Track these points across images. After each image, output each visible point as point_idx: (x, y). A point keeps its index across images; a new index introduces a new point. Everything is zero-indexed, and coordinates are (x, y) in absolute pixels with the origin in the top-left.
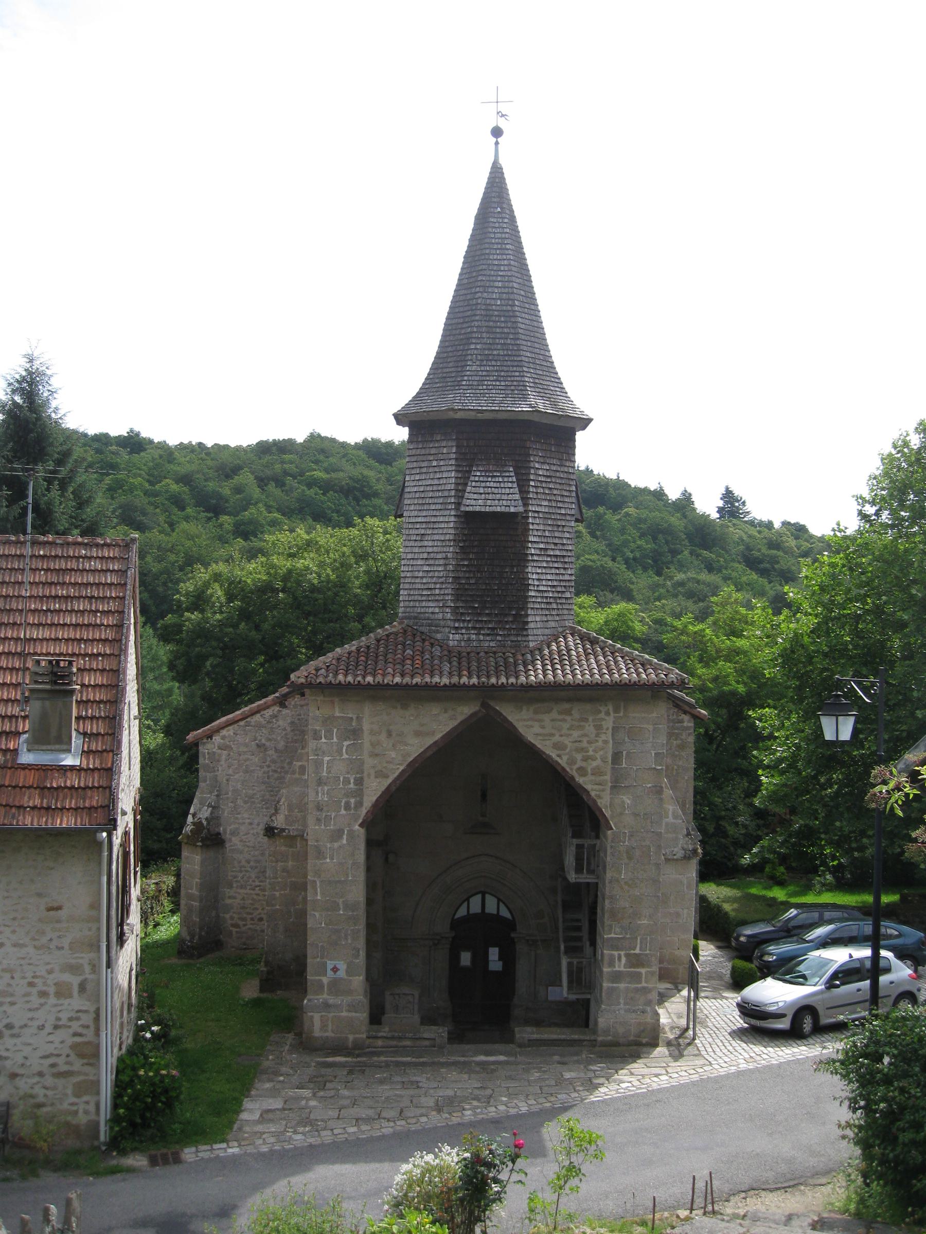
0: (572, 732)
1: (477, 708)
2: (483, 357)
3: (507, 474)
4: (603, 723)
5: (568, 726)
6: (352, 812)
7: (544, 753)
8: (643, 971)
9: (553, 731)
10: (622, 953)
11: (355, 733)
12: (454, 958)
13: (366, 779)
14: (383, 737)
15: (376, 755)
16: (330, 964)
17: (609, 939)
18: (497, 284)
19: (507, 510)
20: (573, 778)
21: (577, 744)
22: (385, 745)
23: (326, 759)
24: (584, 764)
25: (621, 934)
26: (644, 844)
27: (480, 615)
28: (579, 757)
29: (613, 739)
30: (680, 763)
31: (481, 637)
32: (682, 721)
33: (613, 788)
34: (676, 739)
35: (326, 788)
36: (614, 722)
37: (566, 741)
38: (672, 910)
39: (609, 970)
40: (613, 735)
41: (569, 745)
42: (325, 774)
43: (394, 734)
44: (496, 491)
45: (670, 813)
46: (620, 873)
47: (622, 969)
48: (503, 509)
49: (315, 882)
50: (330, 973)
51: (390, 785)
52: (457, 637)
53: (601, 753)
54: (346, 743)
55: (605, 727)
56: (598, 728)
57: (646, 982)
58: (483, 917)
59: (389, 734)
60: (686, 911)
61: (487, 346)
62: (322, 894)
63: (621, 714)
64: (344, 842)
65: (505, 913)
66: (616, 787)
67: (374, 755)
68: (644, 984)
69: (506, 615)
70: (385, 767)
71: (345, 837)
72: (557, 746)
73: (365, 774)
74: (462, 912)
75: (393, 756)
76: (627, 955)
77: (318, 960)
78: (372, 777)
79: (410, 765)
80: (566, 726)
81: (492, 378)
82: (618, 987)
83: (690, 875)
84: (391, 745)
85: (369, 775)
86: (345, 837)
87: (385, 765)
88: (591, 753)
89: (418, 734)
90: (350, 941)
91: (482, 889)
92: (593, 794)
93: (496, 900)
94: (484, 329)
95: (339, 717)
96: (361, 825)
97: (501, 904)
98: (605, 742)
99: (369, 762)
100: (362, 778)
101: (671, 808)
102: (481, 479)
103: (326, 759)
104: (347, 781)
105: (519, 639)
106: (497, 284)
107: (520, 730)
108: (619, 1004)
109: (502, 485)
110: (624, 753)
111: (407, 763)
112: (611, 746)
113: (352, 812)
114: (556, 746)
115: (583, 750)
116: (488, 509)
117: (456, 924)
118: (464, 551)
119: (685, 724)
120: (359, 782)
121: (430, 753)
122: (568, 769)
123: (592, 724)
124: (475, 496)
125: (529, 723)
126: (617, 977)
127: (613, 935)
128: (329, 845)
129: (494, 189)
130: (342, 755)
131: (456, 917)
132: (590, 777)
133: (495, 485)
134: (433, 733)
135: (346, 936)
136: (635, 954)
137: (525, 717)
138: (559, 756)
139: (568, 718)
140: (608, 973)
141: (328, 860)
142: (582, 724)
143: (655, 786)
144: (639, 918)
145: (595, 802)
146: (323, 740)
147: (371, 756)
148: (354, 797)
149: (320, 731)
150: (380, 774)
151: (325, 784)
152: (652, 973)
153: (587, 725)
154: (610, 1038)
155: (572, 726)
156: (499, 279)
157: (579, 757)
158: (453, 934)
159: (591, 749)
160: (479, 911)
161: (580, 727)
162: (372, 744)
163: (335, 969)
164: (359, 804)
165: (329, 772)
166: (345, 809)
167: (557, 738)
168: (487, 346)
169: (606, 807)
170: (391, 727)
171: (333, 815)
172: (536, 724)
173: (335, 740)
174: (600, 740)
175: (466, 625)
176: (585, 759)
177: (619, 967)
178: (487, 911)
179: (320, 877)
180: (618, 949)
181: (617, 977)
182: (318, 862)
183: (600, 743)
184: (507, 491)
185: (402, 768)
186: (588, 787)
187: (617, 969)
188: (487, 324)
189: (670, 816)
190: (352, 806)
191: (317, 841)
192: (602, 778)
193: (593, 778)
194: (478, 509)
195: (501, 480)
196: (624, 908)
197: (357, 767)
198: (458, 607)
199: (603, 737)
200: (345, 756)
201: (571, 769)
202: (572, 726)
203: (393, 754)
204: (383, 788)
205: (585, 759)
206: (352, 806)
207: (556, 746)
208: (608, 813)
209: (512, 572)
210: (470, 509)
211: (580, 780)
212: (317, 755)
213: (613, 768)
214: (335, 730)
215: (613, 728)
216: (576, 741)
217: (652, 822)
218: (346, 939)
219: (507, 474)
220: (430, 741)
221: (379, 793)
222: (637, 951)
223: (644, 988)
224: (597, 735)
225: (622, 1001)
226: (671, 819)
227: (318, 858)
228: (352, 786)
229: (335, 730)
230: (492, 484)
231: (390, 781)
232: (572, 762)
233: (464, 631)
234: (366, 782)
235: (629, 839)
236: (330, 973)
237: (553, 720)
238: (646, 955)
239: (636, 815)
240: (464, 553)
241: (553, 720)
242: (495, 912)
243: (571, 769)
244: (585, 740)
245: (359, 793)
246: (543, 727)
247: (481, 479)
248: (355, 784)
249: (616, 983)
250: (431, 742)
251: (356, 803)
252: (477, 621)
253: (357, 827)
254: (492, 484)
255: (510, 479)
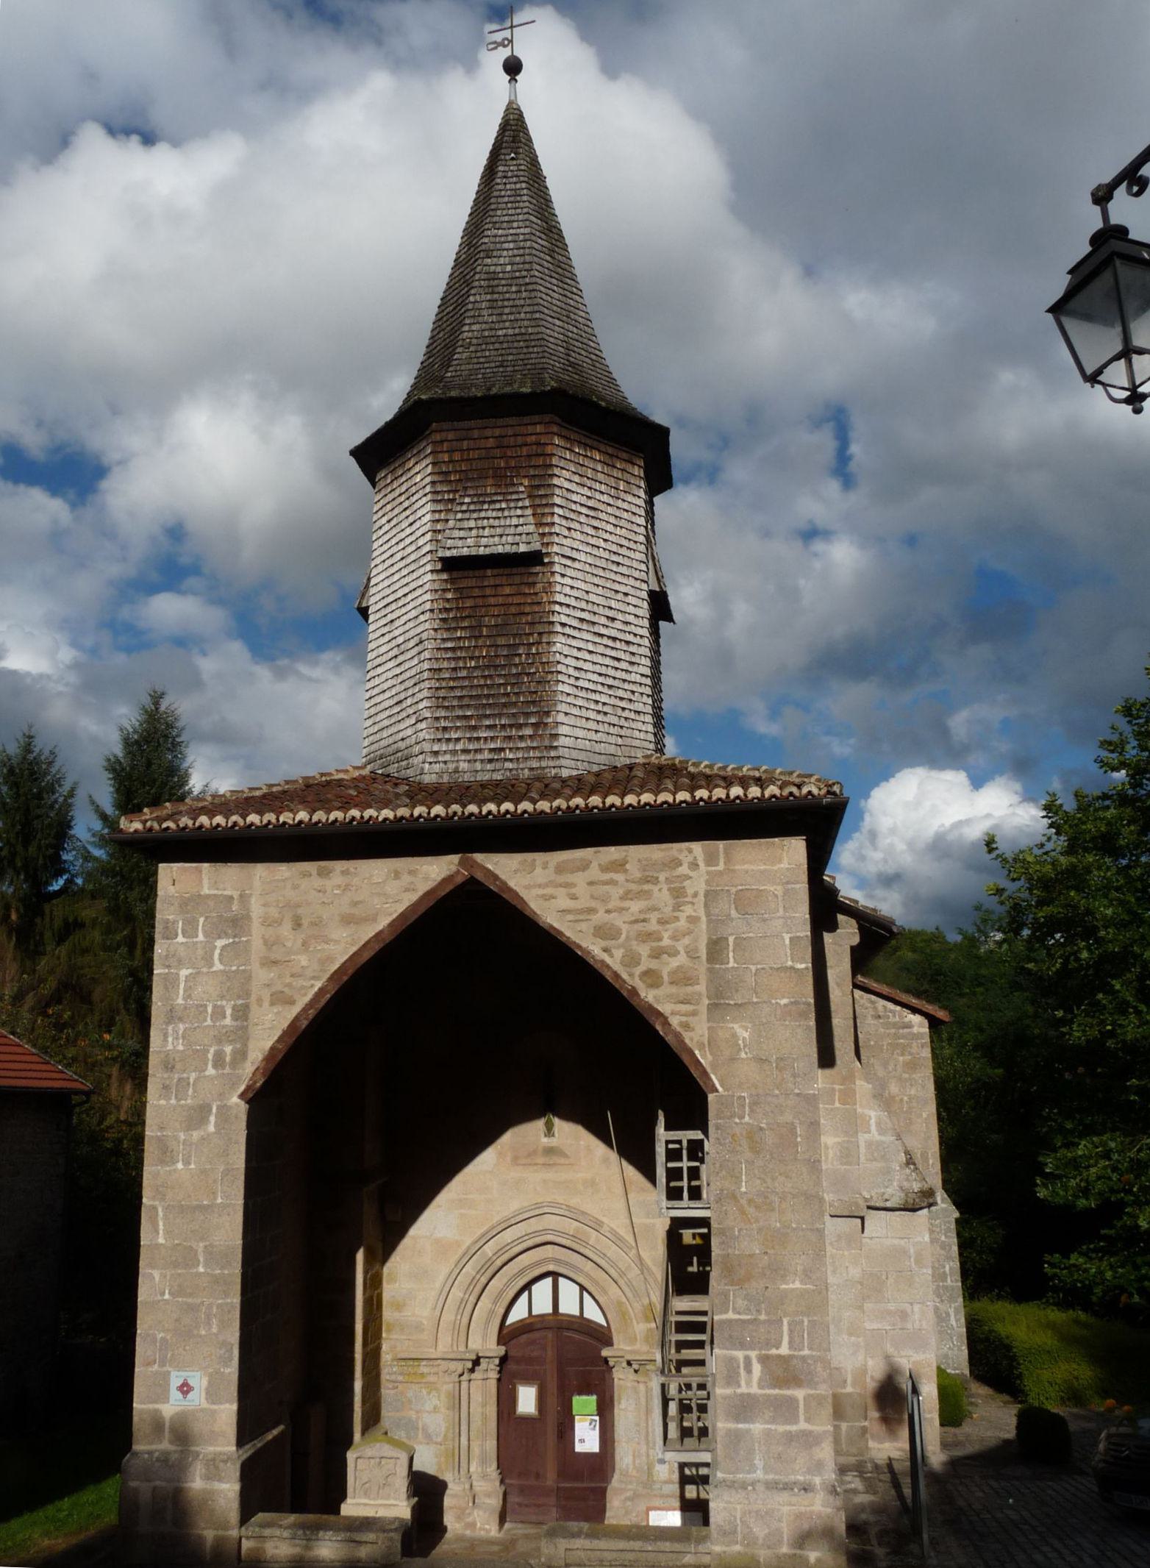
0: (627, 904)
1: (454, 868)
2: (480, 341)
3: (514, 497)
4: (687, 883)
5: (621, 891)
6: (227, 1070)
7: (579, 947)
8: (799, 1394)
9: (593, 904)
10: (753, 1354)
11: (236, 924)
12: (506, 1400)
13: (254, 1007)
14: (286, 930)
15: (275, 962)
16: (175, 1381)
17: (722, 1322)
18: (506, 246)
19: (514, 549)
20: (634, 992)
21: (639, 927)
22: (289, 944)
23: (184, 973)
24: (653, 965)
25: (748, 1311)
26: (781, 1119)
27: (475, 728)
28: (644, 950)
29: (708, 914)
30: (913, 1092)
31: (478, 766)
32: (909, 1026)
33: (713, 1007)
34: (903, 1055)
35: (181, 1026)
36: (707, 882)
37: (619, 921)
38: (892, 1306)
39: (729, 1391)
40: (706, 906)
41: (625, 928)
42: (180, 1001)
43: (305, 922)
44: (496, 523)
45: (873, 1122)
46: (738, 1179)
47: (754, 1390)
48: (508, 549)
49: (155, 1208)
50: (175, 1395)
51: (297, 1018)
52: (437, 767)
53: (686, 941)
54: (220, 943)
55: (690, 891)
56: (678, 893)
57: (808, 1420)
58: (556, 1324)
59: (297, 924)
60: (917, 1308)
61: (487, 326)
62: (168, 1233)
63: (721, 867)
64: (211, 1128)
65: (593, 1313)
66: (717, 1007)
67: (270, 963)
68: (803, 1425)
69: (520, 726)
70: (289, 985)
71: (212, 1119)
72: (605, 932)
73: (253, 998)
74: (519, 1313)
75: (304, 963)
76: (764, 1360)
77: (156, 1367)
78: (266, 1004)
79: (331, 978)
80: (615, 892)
81: (493, 365)
82: (748, 1431)
83: (919, 1239)
84: (300, 942)
85: (260, 1001)
86: (212, 1119)
87: (288, 980)
88: (666, 942)
89: (348, 920)
90: (214, 1330)
91: (551, 1268)
92: (674, 1021)
93: (577, 1288)
94: (484, 305)
95: (208, 896)
96: (242, 1096)
97: (585, 1293)
98: (693, 920)
99: (262, 975)
100: (246, 1008)
101: (873, 1114)
102: (472, 507)
103: (184, 973)
104: (219, 1013)
105: (544, 764)
106: (506, 246)
107: (533, 905)
108: (753, 1469)
109: (506, 513)
110: (731, 939)
111: (327, 975)
112: (704, 926)
113: (227, 1070)
114: (600, 932)
115: (648, 937)
116: (482, 551)
117: (507, 1335)
118: (446, 625)
119: (915, 1030)
120: (242, 1013)
121: (367, 955)
122: (625, 976)
123: (665, 887)
124: (462, 534)
125: (549, 891)
126: (744, 1409)
127: (731, 1315)
128: (182, 1136)
129: (507, 134)
130: (211, 964)
131: (510, 1320)
132: (666, 989)
133: (494, 514)
134: (374, 919)
135: (208, 1317)
136: (779, 1356)
137: (540, 880)
138: (605, 950)
139: (620, 877)
140: (725, 1398)
141: (180, 1166)
142: (646, 887)
143: (796, 1003)
144: (783, 1277)
145: (678, 1036)
146: (180, 939)
147: (263, 965)
148: (231, 1042)
149: (175, 922)
150: (280, 999)
151: (181, 1019)
152: (820, 1400)
153: (656, 889)
154: (738, 1548)
155: (630, 891)
156: (510, 238)
157: (644, 950)
158: (501, 1350)
159: (666, 935)
160: (549, 1310)
161: (646, 895)
162: (266, 942)
163: (185, 1389)
164: (241, 1055)
165: (188, 997)
166: (215, 1066)
167: (600, 917)
168: (487, 326)
169: (701, 1046)
170: (300, 911)
171: (193, 1076)
172: (561, 892)
173: (201, 937)
174: (683, 916)
175: (451, 747)
176: (656, 954)
177: (749, 1383)
178: (562, 1310)
179: (163, 1199)
180: (743, 1346)
181: (744, 1409)
182: (163, 1170)
183: (682, 923)
184: (515, 521)
185: (318, 985)
186: (665, 1008)
187: (743, 1389)
188: (489, 297)
189: (873, 1128)
190: (228, 1059)
191: (162, 1129)
192: (689, 989)
193: (674, 989)
194: (465, 552)
195: (504, 505)
196: (751, 1256)
197: (239, 985)
198: (437, 719)
199: (688, 910)
200: (218, 966)
201: (631, 975)
202: (628, 892)
203: (303, 959)
204: (285, 1025)
205: (656, 954)
206: (228, 1059)
207: (600, 932)
208: (704, 1058)
209: (528, 654)
210: (454, 553)
211: (648, 995)
212: (168, 967)
213: (710, 970)
214: (202, 920)
215: (707, 894)
216: (636, 921)
217: (794, 1076)
218: (209, 1324)
219: (514, 497)
220: (368, 932)
221: (278, 1033)
222: (784, 1350)
223: (806, 1434)
224: (677, 908)
225: (758, 1462)
226: (874, 1134)
227: (162, 1162)
228: (228, 1021)
229: (202, 920)
230: (490, 514)
231: (296, 1010)
232: (631, 960)
233: (447, 757)
234: (255, 1011)
235: (752, 1111)
236: (175, 1395)
237: (591, 883)
238: (804, 1359)
239: (761, 1061)
240: (448, 630)
241: (591, 883)
242: (577, 1313)
243: (631, 975)
244: (654, 917)
245: (241, 1034)
246: (574, 897)
247: (472, 507)
248: (235, 1018)
249: (745, 1421)
250: (372, 934)
251: (234, 1052)
252: (470, 739)
253: (235, 1099)
254: (490, 514)
255: (520, 504)
